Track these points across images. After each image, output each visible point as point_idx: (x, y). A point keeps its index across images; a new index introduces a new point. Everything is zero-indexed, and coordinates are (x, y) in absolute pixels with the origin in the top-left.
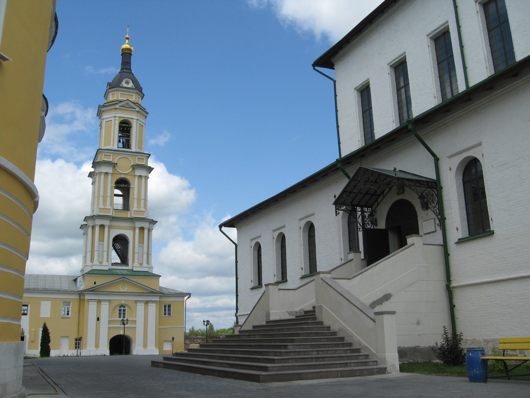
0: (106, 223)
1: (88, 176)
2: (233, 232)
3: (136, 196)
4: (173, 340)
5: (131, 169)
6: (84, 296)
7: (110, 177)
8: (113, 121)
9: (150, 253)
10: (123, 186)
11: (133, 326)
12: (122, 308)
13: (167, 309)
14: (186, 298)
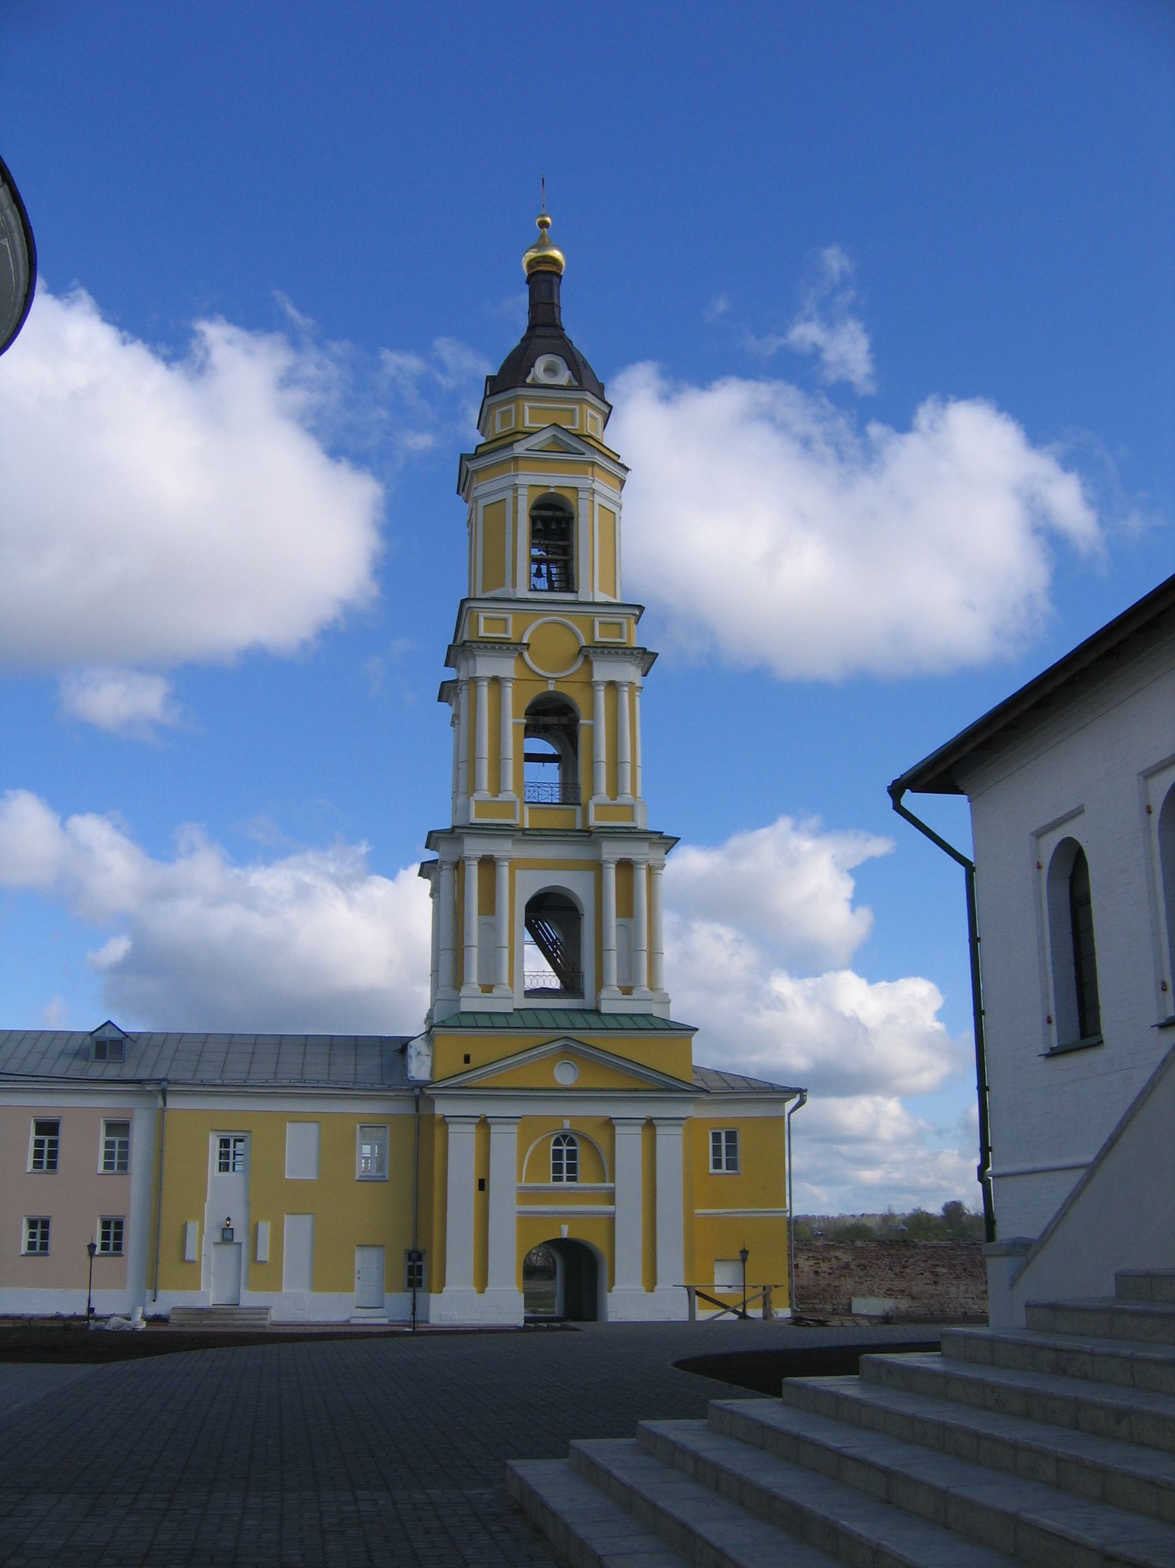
0: (502, 849)
1: (440, 700)
2: (948, 812)
3: (602, 753)
4: (744, 1260)
6: (432, 1103)
8: (510, 502)
10: (551, 720)
13: (727, 1146)
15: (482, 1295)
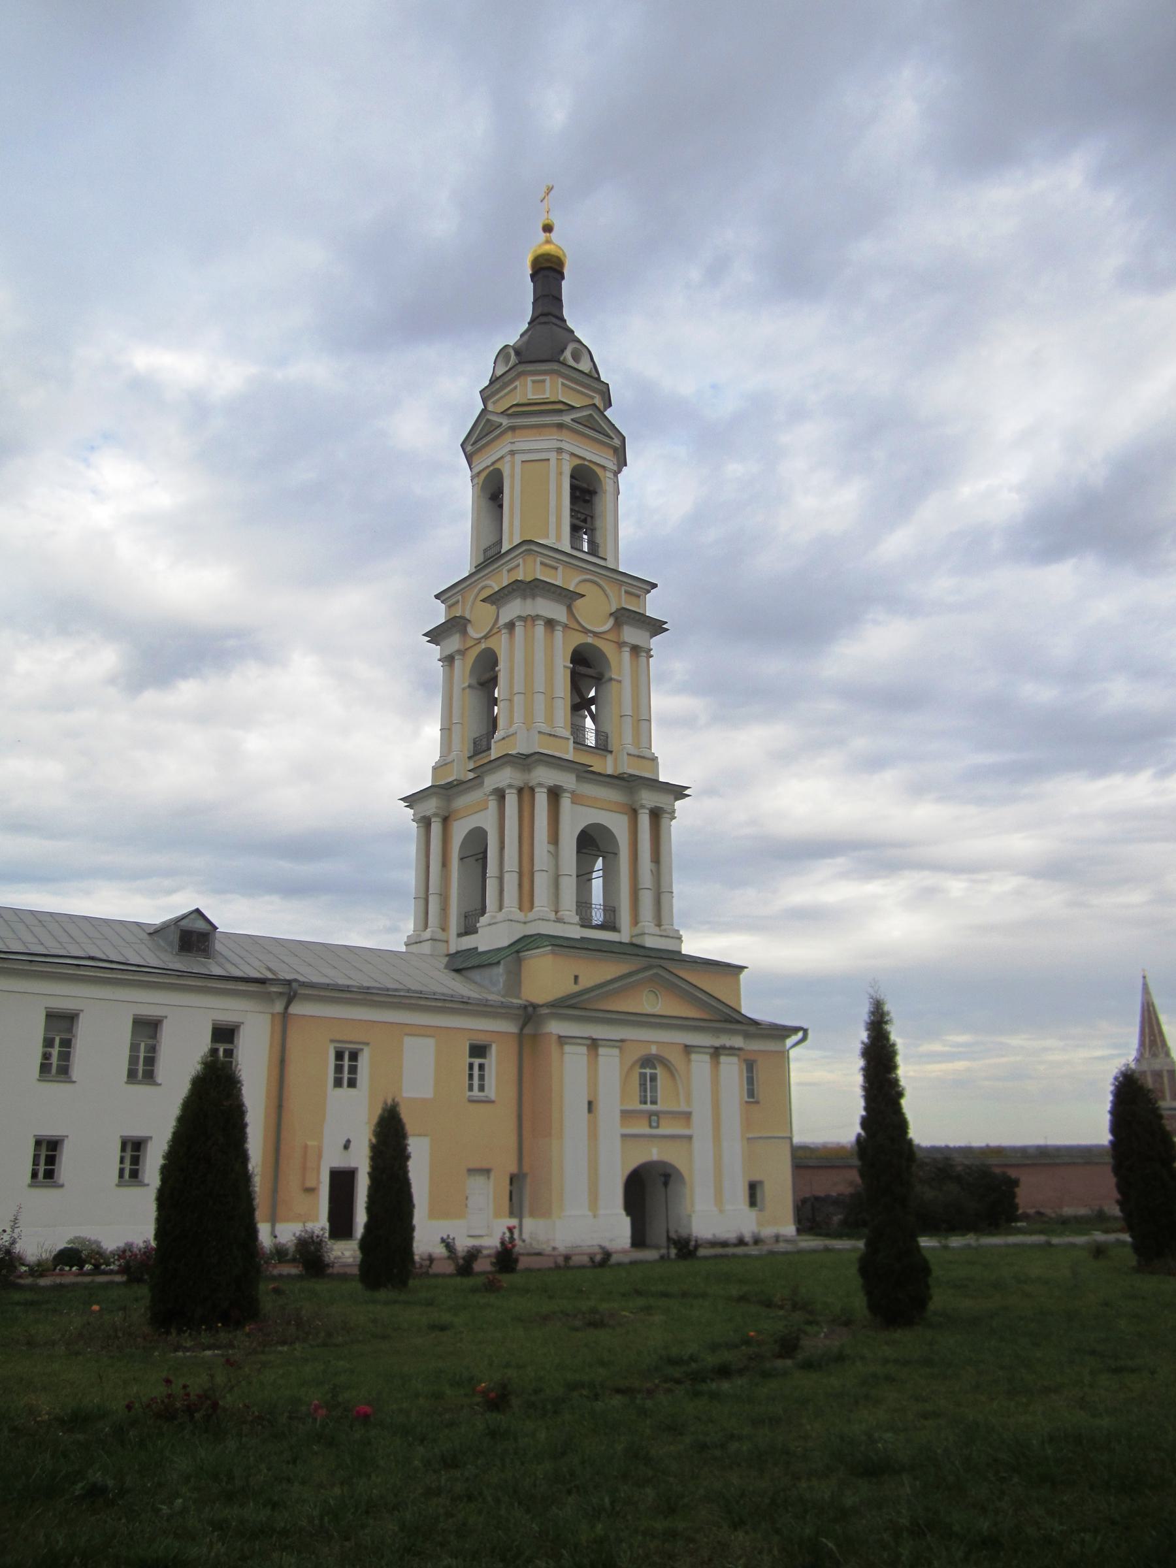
0: (567, 780)
5: (611, 622)
7: (559, 634)
8: (553, 462)
9: (422, 902)
11: (686, 1132)
12: (648, 1071)
14: (790, 1042)
15: (586, 1220)
